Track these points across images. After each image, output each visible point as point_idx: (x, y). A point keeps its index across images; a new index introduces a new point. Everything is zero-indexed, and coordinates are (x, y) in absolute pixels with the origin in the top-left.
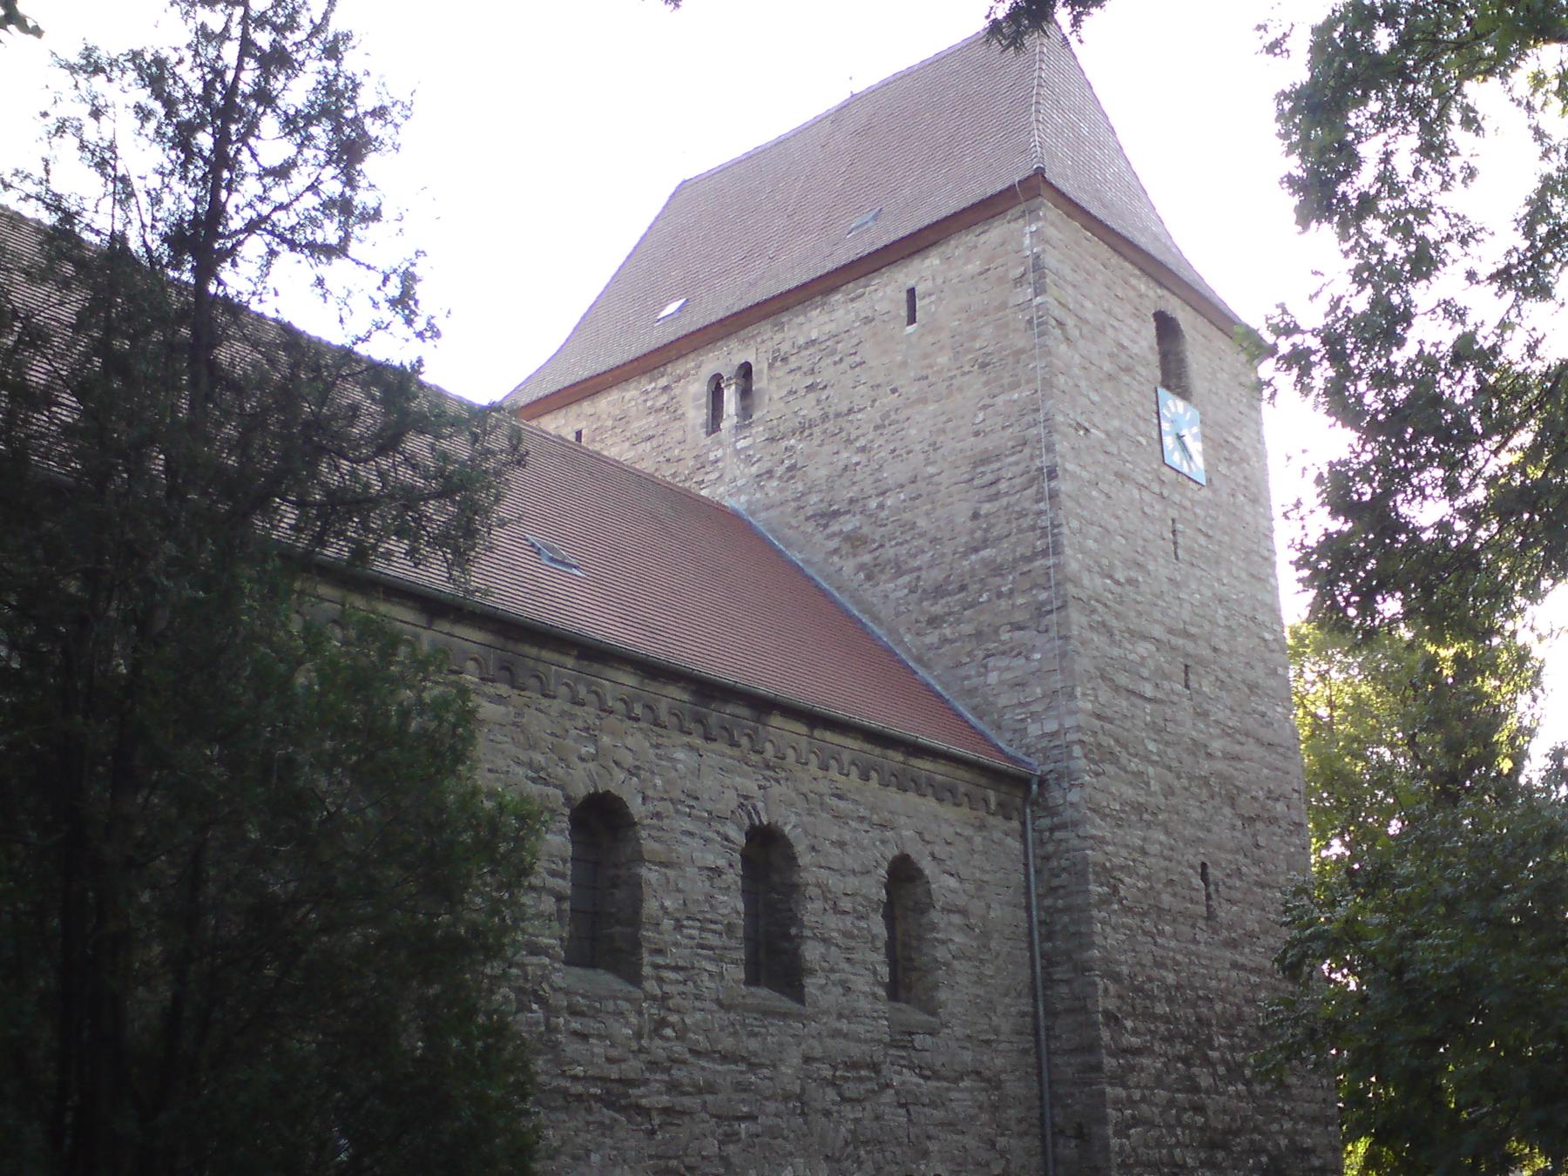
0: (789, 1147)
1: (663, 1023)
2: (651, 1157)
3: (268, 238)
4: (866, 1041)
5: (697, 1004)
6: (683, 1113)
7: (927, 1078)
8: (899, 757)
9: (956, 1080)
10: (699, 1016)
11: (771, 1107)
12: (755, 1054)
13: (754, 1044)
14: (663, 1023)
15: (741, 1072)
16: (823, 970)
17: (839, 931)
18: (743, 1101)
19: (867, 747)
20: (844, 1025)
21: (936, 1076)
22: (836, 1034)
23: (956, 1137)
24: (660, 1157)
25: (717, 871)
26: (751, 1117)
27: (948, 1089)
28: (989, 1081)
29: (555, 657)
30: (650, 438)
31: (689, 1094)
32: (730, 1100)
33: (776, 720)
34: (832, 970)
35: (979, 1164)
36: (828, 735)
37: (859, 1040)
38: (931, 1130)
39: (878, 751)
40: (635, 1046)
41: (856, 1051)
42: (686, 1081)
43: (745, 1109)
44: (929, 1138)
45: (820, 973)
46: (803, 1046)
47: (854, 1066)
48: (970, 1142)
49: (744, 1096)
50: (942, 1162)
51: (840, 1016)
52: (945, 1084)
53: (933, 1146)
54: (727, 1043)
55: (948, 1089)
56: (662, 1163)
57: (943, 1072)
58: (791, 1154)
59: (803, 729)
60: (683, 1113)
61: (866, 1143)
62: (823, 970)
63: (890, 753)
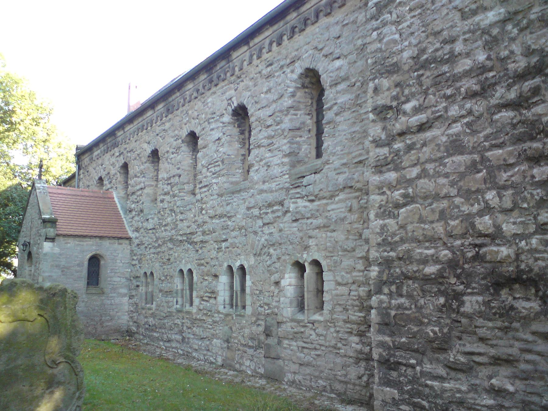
0: (239, 251)
1: (202, 209)
2: (196, 260)
3: (447, 170)
4: (276, 191)
5: (212, 198)
6: (205, 242)
7: (312, 201)
8: (294, 15)
9: (332, 197)
10: (211, 202)
11: (234, 234)
12: (228, 212)
13: (228, 208)
14: (202, 209)
15: (224, 221)
16: (257, 162)
17: (265, 138)
18: (223, 234)
19: (275, 27)
20: (266, 186)
21: (317, 197)
22: (262, 191)
23: (329, 234)
24: (199, 260)
25: (337, 180)
26: (226, 240)
27: (327, 204)
28: (360, 190)
29: (174, 97)
30: (309, 43)
31: (208, 234)
32: (220, 234)
33: (235, 55)
34: (261, 160)
35: (346, 250)
36: (256, 40)
37: (272, 192)
38: (311, 233)
39: (281, 23)
40: (194, 220)
41: (270, 197)
42: (206, 229)
43: (224, 237)
44: (310, 237)
45: (256, 164)
46: (247, 203)
47: (270, 205)
48: (339, 236)
49: (224, 231)
50: (318, 250)
51: (264, 182)
52: (325, 201)
53: (312, 242)
54: (219, 211)
55: (327, 204)
56: (199, 262)
57: (322, 194)
58: (239, 254)
59: (245, 48)
60: (205, 242)
61: (273, 245)
62: (257, 162)
63: (289, 18)
